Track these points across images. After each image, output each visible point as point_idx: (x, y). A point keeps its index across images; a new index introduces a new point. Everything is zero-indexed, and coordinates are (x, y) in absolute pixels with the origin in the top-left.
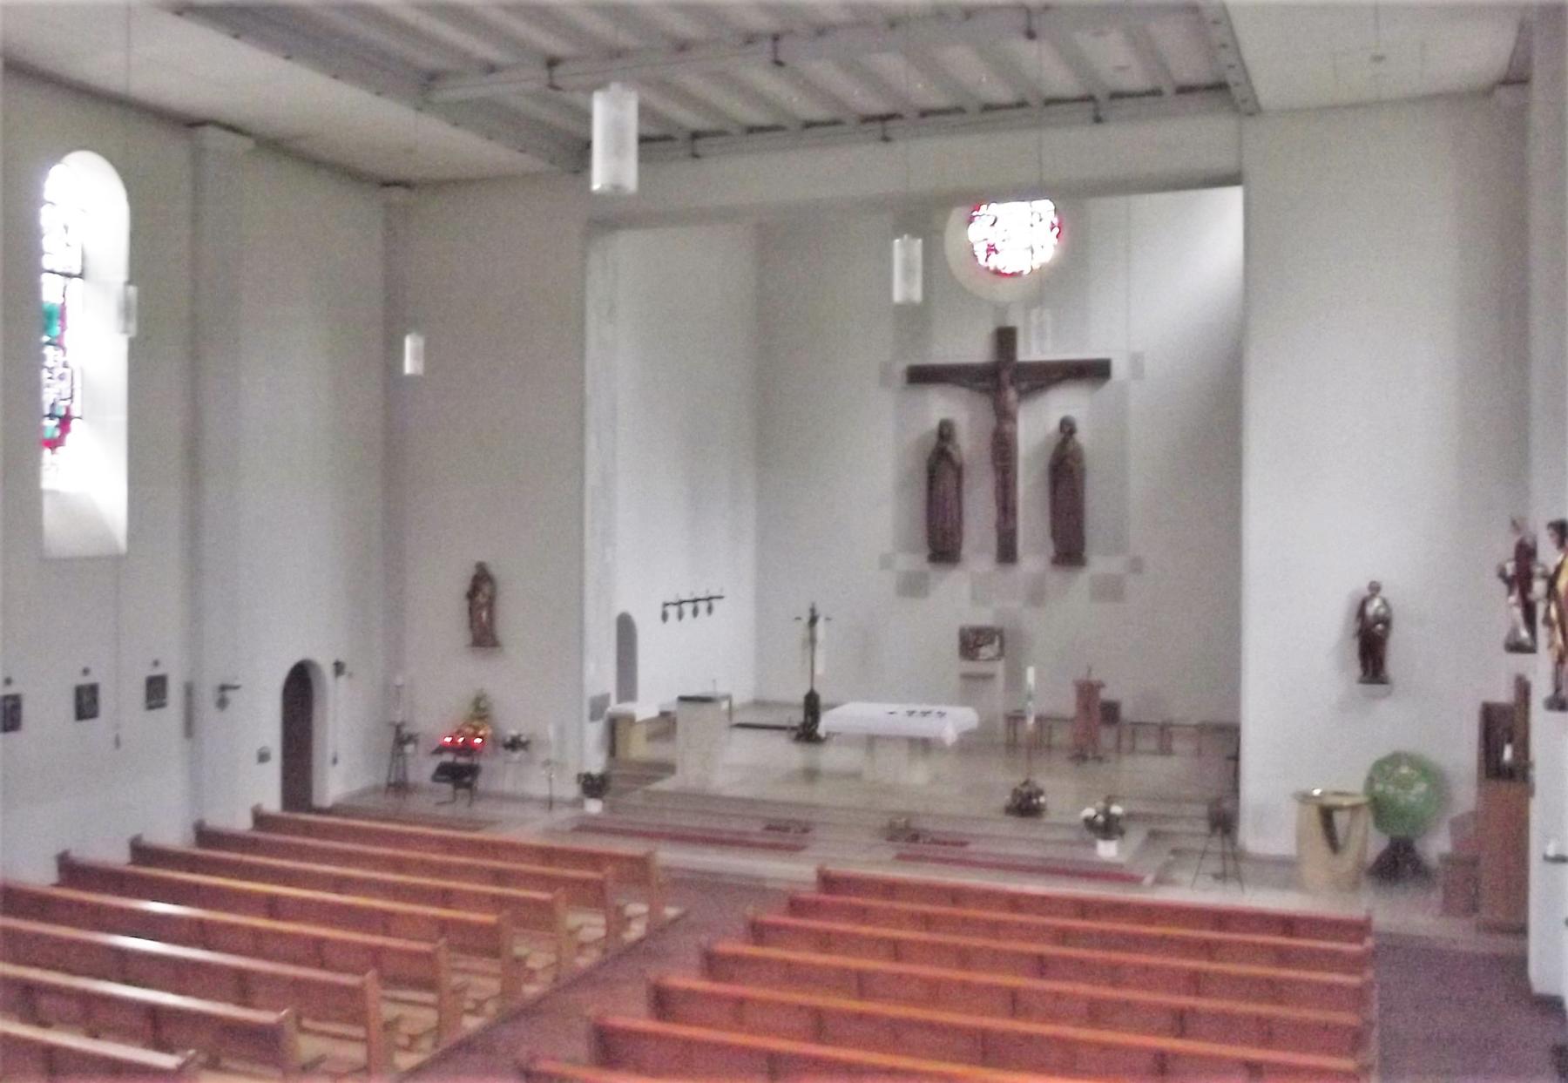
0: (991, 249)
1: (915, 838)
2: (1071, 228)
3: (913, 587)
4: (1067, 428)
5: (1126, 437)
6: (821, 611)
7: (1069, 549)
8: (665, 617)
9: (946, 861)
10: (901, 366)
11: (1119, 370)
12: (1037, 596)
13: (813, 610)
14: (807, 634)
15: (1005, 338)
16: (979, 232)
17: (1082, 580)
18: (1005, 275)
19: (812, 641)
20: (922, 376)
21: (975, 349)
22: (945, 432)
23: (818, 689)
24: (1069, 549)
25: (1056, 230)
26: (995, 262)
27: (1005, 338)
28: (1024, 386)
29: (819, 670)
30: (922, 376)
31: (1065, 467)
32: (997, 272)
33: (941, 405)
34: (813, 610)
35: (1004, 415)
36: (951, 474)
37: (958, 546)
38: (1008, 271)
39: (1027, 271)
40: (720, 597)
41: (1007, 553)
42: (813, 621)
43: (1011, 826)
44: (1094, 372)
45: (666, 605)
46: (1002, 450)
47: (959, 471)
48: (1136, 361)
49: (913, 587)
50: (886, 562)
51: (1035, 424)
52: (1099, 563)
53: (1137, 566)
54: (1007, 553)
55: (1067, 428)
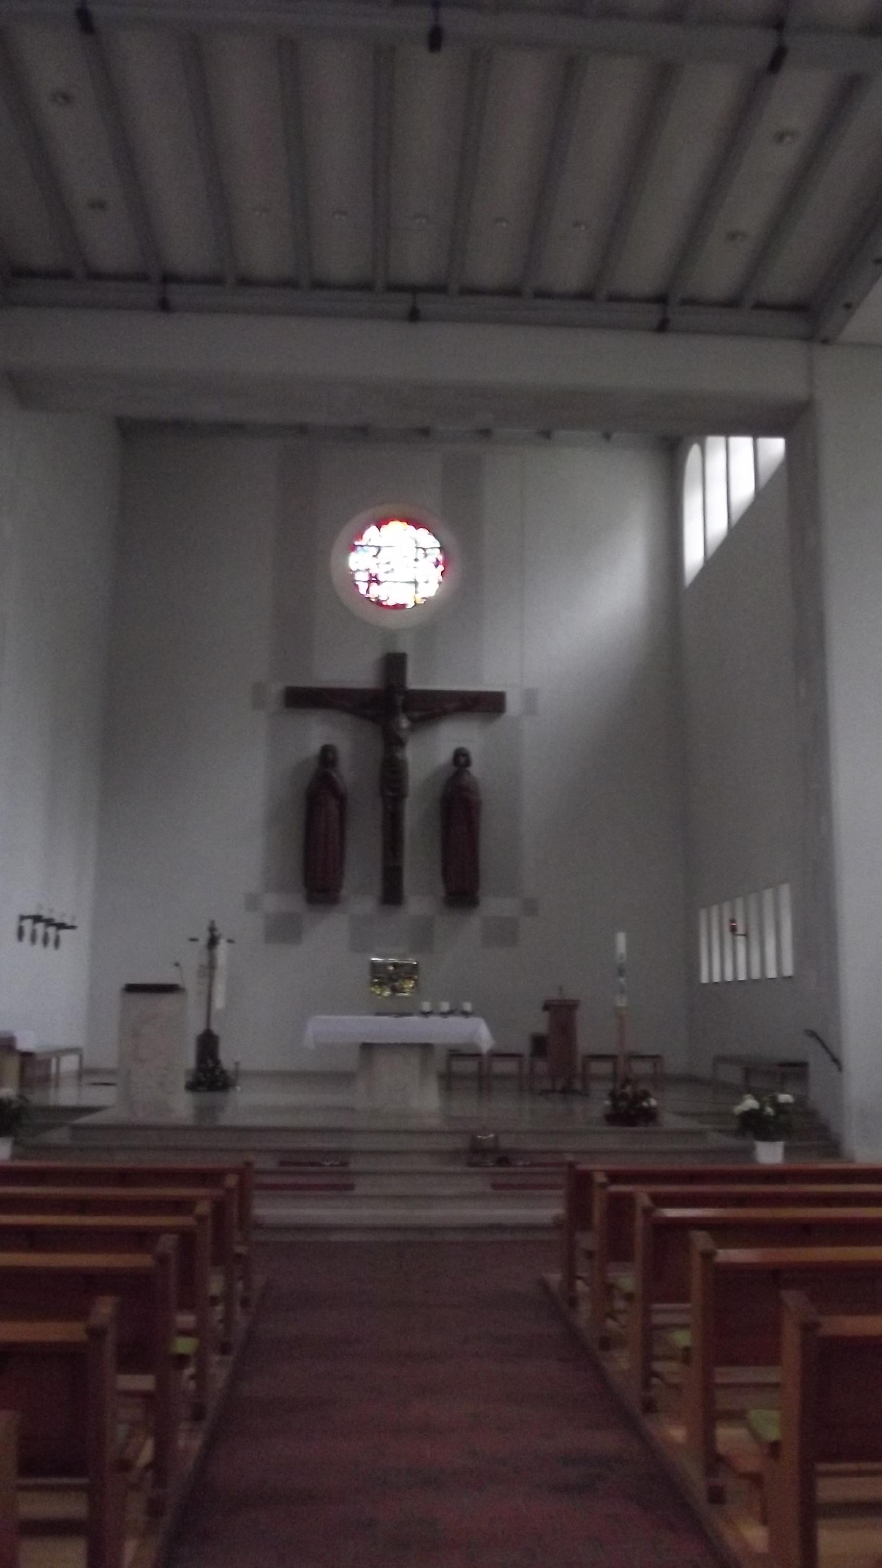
0: (374, 580)
1: (503, 1159)
2: (465, 558)
3: (284, 931)
4: (461, 759)
5: (527, 768)
6: (223, 930)
7: (461, 891)
8: (20, 934)
9: (374, 1229)
10: (276, 688)
11: (513, 705)
12: (423, 937)
13: (212, 929)
14: (205, 960)
15: (394, 664)
16: (359, 562)
17: (473, 924)
18: (388, 606)
19: (211, 966)
20: (303, 699)
21: (358, 672)
22: (327, 756)
23: (215, 1028)
24: (461, 891)
25: (441, 568)
26: (376, 592)
27: (394, 664)
28: (417, 714)
29: (219, 1002)
30: (303, 699)
31: (459, 802)
32: (379, 603)
33: (317, 732)
34: (212, 929)
35: (393, 742)
36: (333, 805)
37: (338, 887)
38: (391, 603)
39: (411, 605)
40: (73, 927)
41: (392, 894)
42: (213, 942)
43: (615, 1139)
44: (488, 705)
45: (23, 918)
46: (392, 778)
47: (341, 799)
48: (530, 697)
49: (284, 931)
50: (252, 903)
51: (428, 754)
52: (493, 905)
53: (531, 908)
54: (392, 894)
55: (461, 759)
